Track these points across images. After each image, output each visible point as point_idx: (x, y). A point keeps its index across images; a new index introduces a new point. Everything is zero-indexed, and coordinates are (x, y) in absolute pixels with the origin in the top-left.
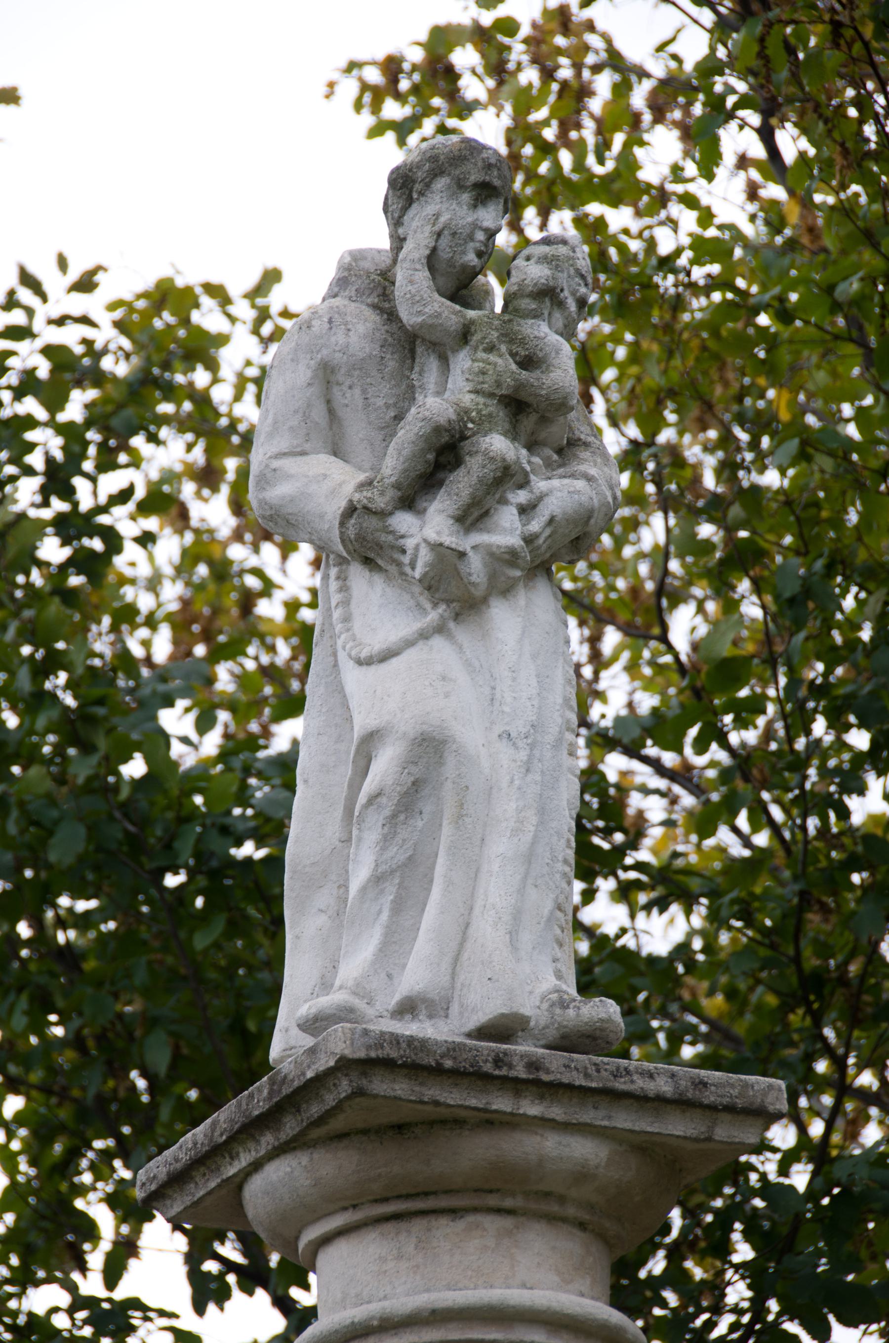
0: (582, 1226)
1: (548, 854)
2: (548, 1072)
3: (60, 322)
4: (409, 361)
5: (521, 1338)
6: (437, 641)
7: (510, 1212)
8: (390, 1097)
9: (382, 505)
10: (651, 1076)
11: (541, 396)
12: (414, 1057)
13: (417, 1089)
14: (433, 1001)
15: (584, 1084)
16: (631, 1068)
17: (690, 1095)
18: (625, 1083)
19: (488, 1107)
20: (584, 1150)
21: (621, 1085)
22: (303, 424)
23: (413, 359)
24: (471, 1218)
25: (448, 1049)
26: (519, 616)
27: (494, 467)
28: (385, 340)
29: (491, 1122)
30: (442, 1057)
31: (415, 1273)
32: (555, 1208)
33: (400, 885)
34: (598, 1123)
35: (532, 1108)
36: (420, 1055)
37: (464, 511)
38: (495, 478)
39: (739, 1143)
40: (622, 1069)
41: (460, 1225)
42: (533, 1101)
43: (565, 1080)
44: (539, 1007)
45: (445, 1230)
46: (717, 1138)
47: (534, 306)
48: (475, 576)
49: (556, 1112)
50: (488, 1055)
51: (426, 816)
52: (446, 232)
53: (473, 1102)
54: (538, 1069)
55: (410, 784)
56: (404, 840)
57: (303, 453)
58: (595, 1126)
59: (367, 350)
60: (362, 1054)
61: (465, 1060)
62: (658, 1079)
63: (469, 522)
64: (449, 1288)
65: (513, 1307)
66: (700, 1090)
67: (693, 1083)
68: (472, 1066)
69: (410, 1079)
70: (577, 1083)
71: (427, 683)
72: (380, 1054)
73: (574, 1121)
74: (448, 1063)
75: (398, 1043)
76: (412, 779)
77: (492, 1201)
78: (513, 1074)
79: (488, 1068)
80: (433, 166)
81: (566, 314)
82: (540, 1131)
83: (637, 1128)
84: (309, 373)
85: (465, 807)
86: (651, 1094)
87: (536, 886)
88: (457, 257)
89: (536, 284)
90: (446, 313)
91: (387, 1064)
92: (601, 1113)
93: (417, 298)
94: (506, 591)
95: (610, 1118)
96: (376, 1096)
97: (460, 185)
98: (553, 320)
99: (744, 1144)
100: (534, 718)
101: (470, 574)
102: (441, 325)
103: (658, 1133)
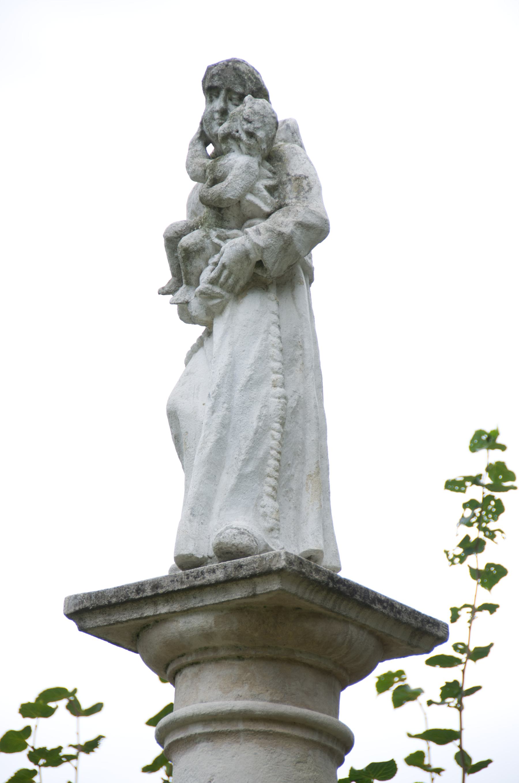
0: (240, 658)
2: (162, 587)
8: (95, 627)
11: (209, 200)
12: (97, 603)
13: (107, 618)
16: (205, 571)
17: (232, 575)
18: (200, 580)
20: (197, 622)
21: (198, 582)
25: (115, 593)
30: (111, 598)
32: (211, 655)
35: (163, 609)
36: (101, 600)
43: (171, 589)
46: (258, 593)
48: (194, 312)
49: (176, 607)
53: (135, 616)
54: (157, 588)
58: (198, 607)
61: (122, 596)
66: (238, 571)
69: (103, 614)
72: (81, 607)
73: (186, 609)
74: (114, 600)
78: (145, 594)
79: (133, 596)
82: (176, 619)
83: (217, 602)
87: (228, 473)
92: (198, 600)
99: (273, 591)
101: (191, 312)
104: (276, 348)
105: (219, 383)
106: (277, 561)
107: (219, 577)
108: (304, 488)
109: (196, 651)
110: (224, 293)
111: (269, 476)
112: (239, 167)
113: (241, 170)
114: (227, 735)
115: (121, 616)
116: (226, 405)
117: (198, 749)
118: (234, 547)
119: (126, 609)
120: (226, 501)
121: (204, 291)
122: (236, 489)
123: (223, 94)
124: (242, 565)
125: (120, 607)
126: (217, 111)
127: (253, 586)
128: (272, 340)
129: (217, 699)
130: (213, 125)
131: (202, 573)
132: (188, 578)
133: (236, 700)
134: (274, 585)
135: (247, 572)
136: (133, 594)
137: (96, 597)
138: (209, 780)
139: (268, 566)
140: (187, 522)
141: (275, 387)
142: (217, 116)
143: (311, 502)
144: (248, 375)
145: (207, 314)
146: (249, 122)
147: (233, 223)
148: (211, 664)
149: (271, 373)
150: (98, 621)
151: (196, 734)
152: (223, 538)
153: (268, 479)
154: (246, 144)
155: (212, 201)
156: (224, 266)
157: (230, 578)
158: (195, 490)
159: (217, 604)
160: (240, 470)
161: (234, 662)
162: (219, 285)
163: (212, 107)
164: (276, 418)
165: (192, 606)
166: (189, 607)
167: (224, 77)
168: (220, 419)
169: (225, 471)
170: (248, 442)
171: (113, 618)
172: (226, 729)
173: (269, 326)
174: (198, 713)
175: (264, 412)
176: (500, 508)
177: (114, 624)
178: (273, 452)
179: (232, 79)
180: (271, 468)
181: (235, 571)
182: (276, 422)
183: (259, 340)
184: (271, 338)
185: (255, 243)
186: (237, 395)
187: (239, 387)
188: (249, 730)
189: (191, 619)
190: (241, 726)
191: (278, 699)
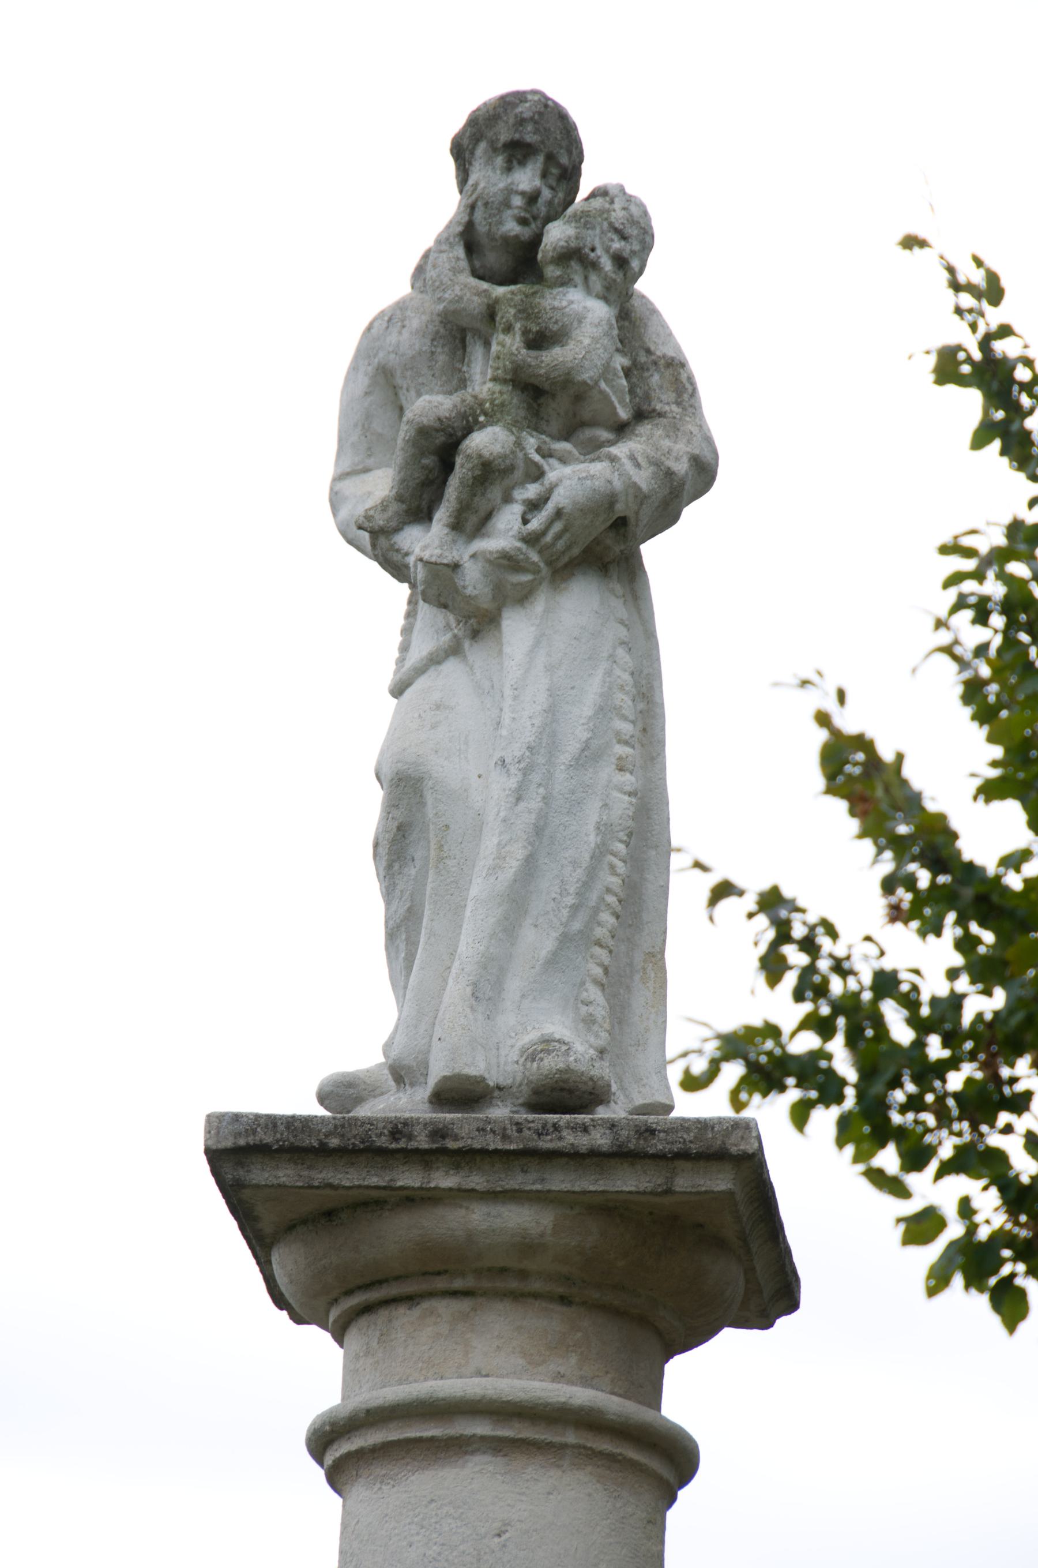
0: (564, 1300)
1: (557, 889)
2: (456, 1138)
4: (459, 353)
5: (461, 1432)
6: (451, 667)
7: (467, 1293)
9: (381, 523)
10: (585, 1129)
11: (541, 375)
12: (292, 1140)
13: (305, 1173)
14: (409, 1068)
15: (500, 1147)
16: (561, 1123)
17: (631, 1146)
18: (551, 1140)
19: (392, 1184)
20: (517, 1219)
21: (546, 1144)
22: (363, 438)
23: (464, 347)
24: (426, 1305)
25: (336, 1127)
26: (532, 625)
27: (471, 465)
28: (437, 332)
30: (326, 1136)
31: (376, 1369)
32: (514, 1284)
33: (407, 939)
34: (528, 1188)
35: (445, 1180)
36: (300, 1136)
37: (456, 518)
38: (474, 478)
39: (706, 1192)
40: (549, 1126)
41: (416, 1312)
42: (447, 1173)
44: (517, 1062)
45: (404, 1316)
46: (678, 1189)
47: (558, 273)
49: (477, 1181)
50: (384, 1128)
51: (418, 863)
52: (479, 203)
53: (374, 1181)
55: (395, 830)
56: (402, 891)
57: (366, 470)
59: (417, 347)
60: (228, 1143)
61: (355, 1137)
62: (593, 1132)
63: (469, 526)
64: (400, 1382)
65: (443, 1399)
66: (645, 1139)
67: (637, 1132)
68: (363, 1142)
69: (296, 1164)
70: (492, 1147)
71: (416, 715)
72: (251, 1140)
73: (499, 1189)
74: (334, 1142)
75: (275, 1126)
76: (396, 824)
77: (440, 1283)
78: (412, 1145)
79: (383, 1142)
80: (474, 130)
81: (603, 275)
82: (465, 1204)
83: (577, 1189)
84: (366, 381)
85: (446, 848)
86: (583, 1150)
87: (536, 926)
88: (494, 229)
89: (555, 249)
90: (468, 295)
91: (261, 1150)
92: (532, 1176)
93: (437, 284)
94: (523, 597)
95: (542, 1180)
96: (258, 1186)
97: (494, 149)
98: (591, 284)
99: (713, 1192)
100: (533, 738)
101: (464, 587)
102: (464, 309)
103: (603, 1192)
104: (627, 693)
105: (533, 744)
106: (742, 1138)
107: (599, 1142)
108: (637, 977)
109: (479, 1272)
110: (542, 565)
111: (599, 944)
112: (596, 321)
113: (600, 329)
114: (539, 1448)
115: (340, 1176)
116: (541, 790)
117: (470, 1465)
118: (591, 1083)
119: (353, 1164)
120: (535, 982)
121: (513, 553)
122: (553, 962)
123: (541, 158)
124: (655, 1130)
125: (341, 1157)
126: (523, 193)
127: (668, 1175)
128: (619, 677)
129: (515, 1373)
130: (504, 217)
131: (556, 1127)
132: (519, 1131)
133: (553, 1381)
134: (719, 1182)
135: (668, 1147)
136: (383, 1138)
137: (288, 1128)
138: (497, 1532)
139: (719, 1142)
140: (468, 1010)
141: (620, 770)
142: (517, 201)
143: (653, 1007)
144: (584, 739)
145: (494, 598)
146: (624, 237)
147: (555, 426)
148: (502, 1300)
149: (615, 741)
150: (281, 1174)
151: (474, 1435)
152: (576, 1061)
153: (597, 950)
154: (606, 277)
155: (548, 379)
156: (559, 513)
157: (625, 1150)
158: (481, 948)
159: (574, 1192)
160: (566, 925)
161: (551, 1307)
162: (538, 547)
163: (509, 180)
164: (622, 833)
165: (517, 1187)
166: (507, 1187)
167: (545, 129)
168: (533, 816)
169: (529, 921)
170: (579, 871)
171: (320, 1176)
172: (543, 1437)
173: (614, 648)
174: (494, 1397)
175: (605, 818)
177: (318, 1187)
178: (611, 899)
179: (559, 137)
180: (604, 930)
181: (639, 1138)
182: (621, 841)
183: (600, 673)
184: (618, 672)
185: (635, 483)
186: (560, 774)
187: (564, 758)
188: (585, 1447)
189: (503, 1209)
190: (571, 1437)
191: (621, 1392)
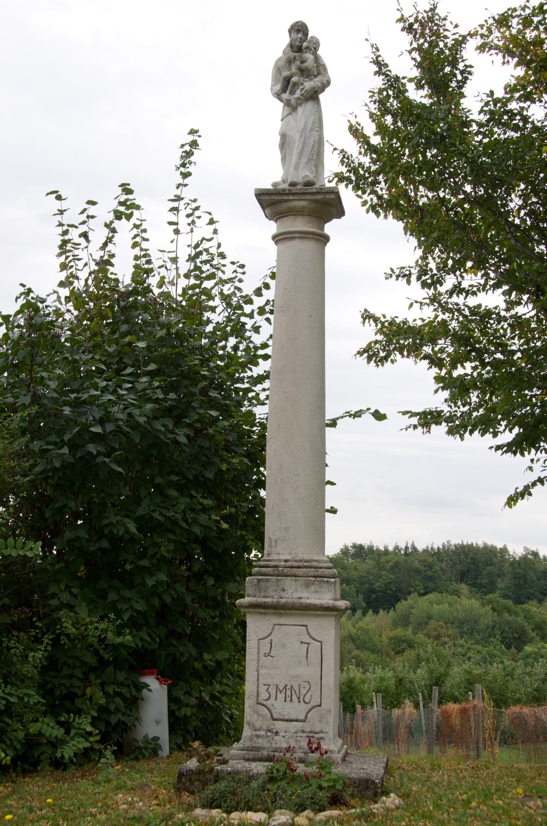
3: (454, 34)
6: (290, 116)
20: (302, 203)
29: (286, 201)
35: (291, 198)
45: (285, 219)
49: (296, 198)
94: (301, 104)
122: (307, 163)
176: (193, 154)
187: (308, 130)
190: (311, 236)
